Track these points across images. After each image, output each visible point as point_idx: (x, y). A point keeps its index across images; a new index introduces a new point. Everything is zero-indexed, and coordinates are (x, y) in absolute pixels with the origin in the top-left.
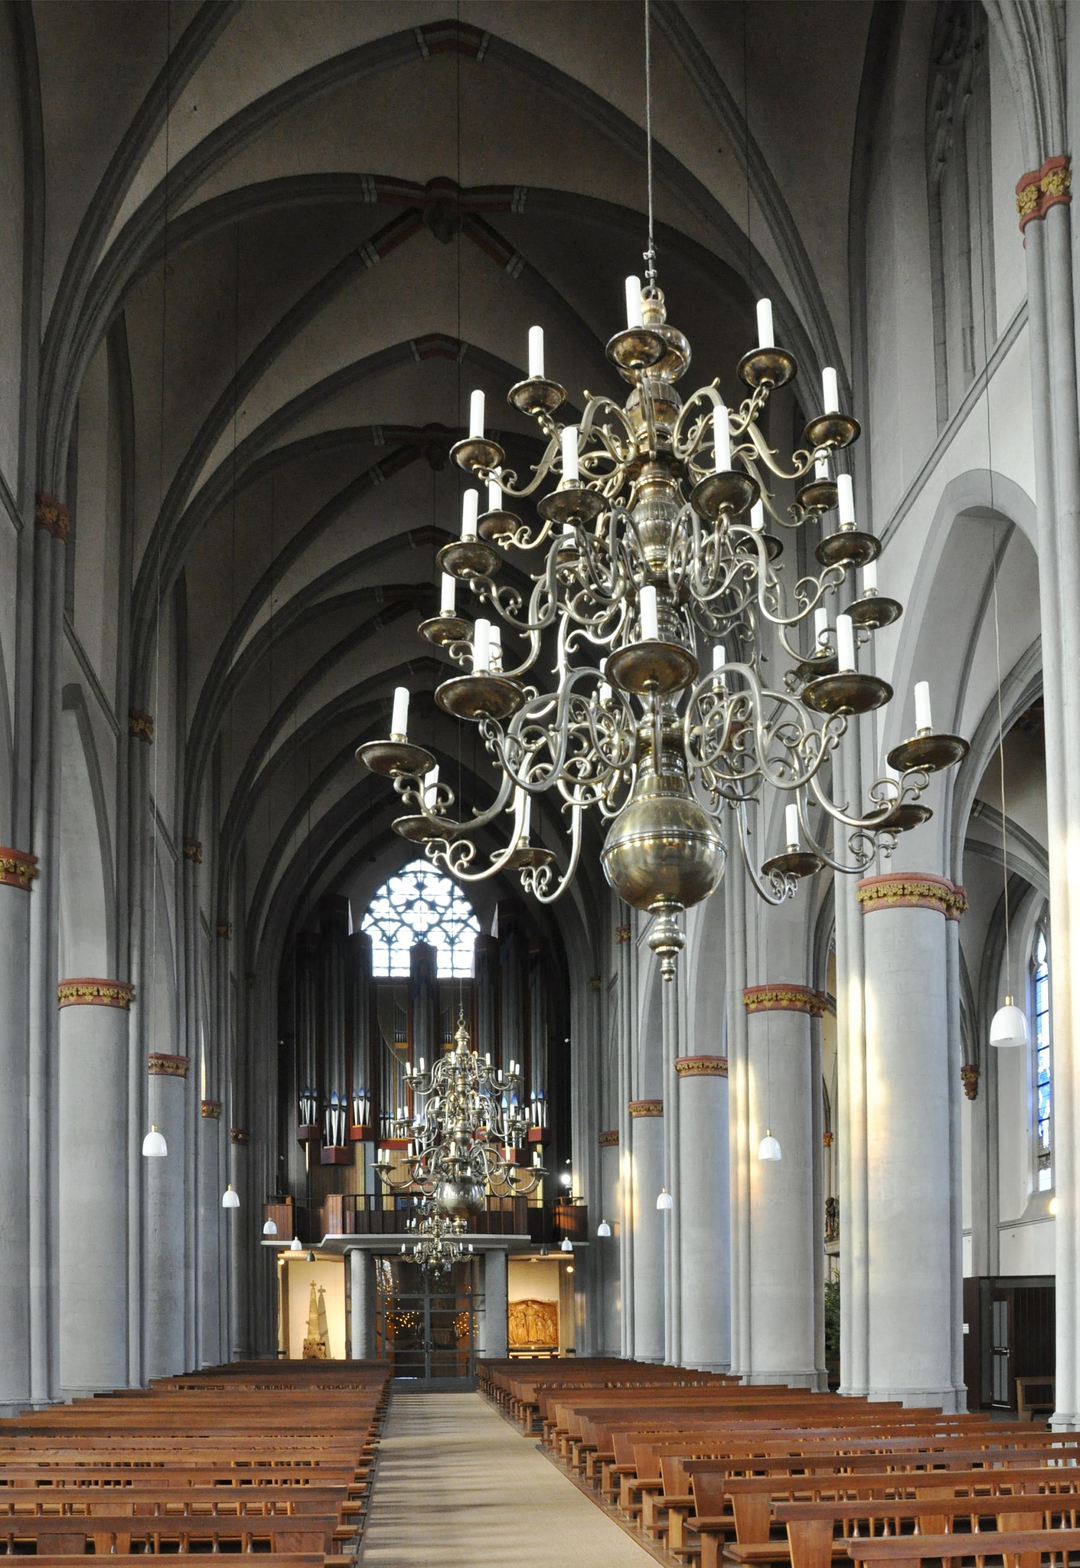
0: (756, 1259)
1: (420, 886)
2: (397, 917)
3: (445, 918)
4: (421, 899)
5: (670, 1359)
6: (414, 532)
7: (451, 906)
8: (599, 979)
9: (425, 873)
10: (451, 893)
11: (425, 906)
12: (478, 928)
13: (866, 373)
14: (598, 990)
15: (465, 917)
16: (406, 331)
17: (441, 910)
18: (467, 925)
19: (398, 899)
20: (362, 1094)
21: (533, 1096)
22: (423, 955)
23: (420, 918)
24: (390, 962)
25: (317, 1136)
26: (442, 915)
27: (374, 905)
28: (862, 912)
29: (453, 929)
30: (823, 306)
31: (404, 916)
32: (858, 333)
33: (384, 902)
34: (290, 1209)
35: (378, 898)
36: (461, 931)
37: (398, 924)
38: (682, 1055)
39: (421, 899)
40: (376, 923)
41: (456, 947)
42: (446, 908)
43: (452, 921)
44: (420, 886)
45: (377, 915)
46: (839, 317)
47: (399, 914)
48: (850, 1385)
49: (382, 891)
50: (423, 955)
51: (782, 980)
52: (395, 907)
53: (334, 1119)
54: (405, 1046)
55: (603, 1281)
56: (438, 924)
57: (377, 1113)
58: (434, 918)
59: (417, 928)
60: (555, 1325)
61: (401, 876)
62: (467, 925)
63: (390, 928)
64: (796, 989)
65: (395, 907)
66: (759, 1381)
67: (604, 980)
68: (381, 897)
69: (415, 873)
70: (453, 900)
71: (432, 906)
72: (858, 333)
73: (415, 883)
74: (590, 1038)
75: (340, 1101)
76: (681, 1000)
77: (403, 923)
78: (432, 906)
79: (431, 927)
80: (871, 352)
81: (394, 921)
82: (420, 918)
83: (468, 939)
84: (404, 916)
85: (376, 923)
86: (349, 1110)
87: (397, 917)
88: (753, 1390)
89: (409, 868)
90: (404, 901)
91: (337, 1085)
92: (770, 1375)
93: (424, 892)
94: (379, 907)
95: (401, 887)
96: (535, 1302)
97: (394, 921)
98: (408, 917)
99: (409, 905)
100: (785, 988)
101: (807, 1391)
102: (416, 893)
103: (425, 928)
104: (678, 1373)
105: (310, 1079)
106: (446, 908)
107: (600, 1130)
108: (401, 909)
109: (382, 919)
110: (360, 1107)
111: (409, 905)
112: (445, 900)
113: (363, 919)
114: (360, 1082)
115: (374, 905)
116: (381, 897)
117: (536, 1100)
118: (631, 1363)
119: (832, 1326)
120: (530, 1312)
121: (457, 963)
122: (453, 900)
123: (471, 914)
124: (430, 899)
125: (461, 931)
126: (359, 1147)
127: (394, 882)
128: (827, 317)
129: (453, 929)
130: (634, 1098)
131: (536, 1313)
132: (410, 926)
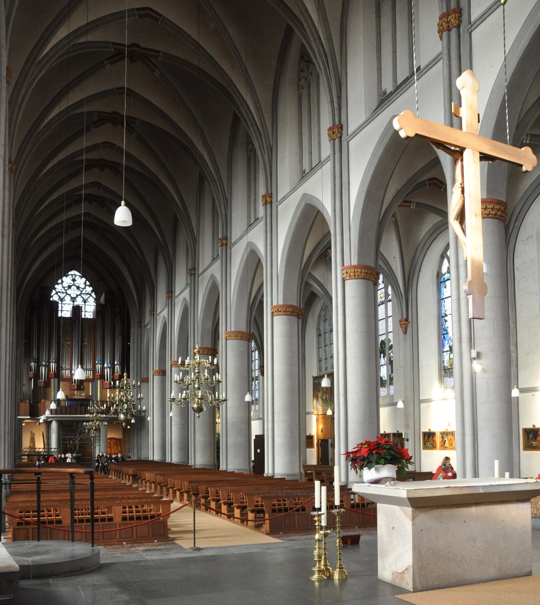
0: (197, 429)
1: (74, 280)
2: (64, 291)
3: (83, 292)
4: (74, 285)
5: (168, 460)
6: (91, 183)
7: (85, 288)
8: (141, 323)
9: (76, 275)
10: (85, 283)
11: (75, 288)
12: (95, 297)
13: (231, 196)
14: (141, 327)
15: (90, 293)
16: (99, 140)
17: (81, 290)
18: (91, 296)
19: (65, 285)
20: (54, 361)
21: (116, 363)
22: (77, 310)
23: (73, 292)
24: (65, 311)
25: (37, 375)
26: (82, 291)
27: (56, 286)
28: (226, 339)
29: (86, 297)
30: (221, 176)
31: (67, 291)
32: (229, 184)
33: (60, 286)
34: (28, 404)
35: (58, 284)
36: (88, 298)
37: (65, 294)
38: (173, 360)
39: (74, 285)
40: (57, 293)
41: (87, 304)
42: (83, 289)
43: (85, 294)
44: (74, 280)
45: (57, 291)
46: (225, 180)
47: (66, 290)
48: (223, 467)
49: (60, 281)
50: (77, 310)
51: (205, 346)
52: (64, 288)
53: (43, 370)
54: (69, 343)
55: (141, 432)
56: (80, 295)
57: (59, 368)
58: (79, 293)
59: (72, 296)
60: (121, 447)
61: (66, 276)
62: (91, 296)
63: (62, 296)
64: (209, 349)
65: (64, 288)
66: (198, 467)
67: (143, 323)
68: (59, 283)
69: (72, 275)
70: (86, 286)
71: (78, 288)
72: (229, 184)
73: (72, 278)
74: (137, 343)
75: (46, 363)
76: (173, 342)
77: (67, 294)
78: (78, 288)
79: (77, 296)
80: (233, 191)
81: (64, 293)
82: (73, 292)
83: (91, 302)
84: (67, 291)
85: (57, 293)
86: (49, 366)
87: (64, 291)
88: (195, 469)
89: (70, 273)
90: (67, 285)
91: (44, 357)
92: (201, 465)
93: (75, 283)
94: (59, 287)
95: (67, 280)
96: (114, 438)
97: (64, 293)
98: (68, 292)
99: (70, 287)
100: (206, 348)
101: (211, 469)
102: (72, 282)
103: (75, 296)
104: (171, 465)
105: (35, 355)
106: (83, 289)
107: (141, 377)
108: (66, 288)
109: (59, 292)
110: (53, 365)
111: (70, 287)
112: (82, 286)
113: (52, 292)
114: (53, 356)
115: (56, 286)
116: (59, 283)
117: (117, 364)
118: (153, 462)
119: (218, 448)
120: (112, 442)
121: (89, 311)
122: (86, 286)
123: (92, 291)
124: (77, 285)
125: (88, 298)
126: (52, 380)
127: (64, 278)
128: (222, 180)
129: (86, 297)
130: (155, 369)
131: (114, 443)
132: (70, 295)
